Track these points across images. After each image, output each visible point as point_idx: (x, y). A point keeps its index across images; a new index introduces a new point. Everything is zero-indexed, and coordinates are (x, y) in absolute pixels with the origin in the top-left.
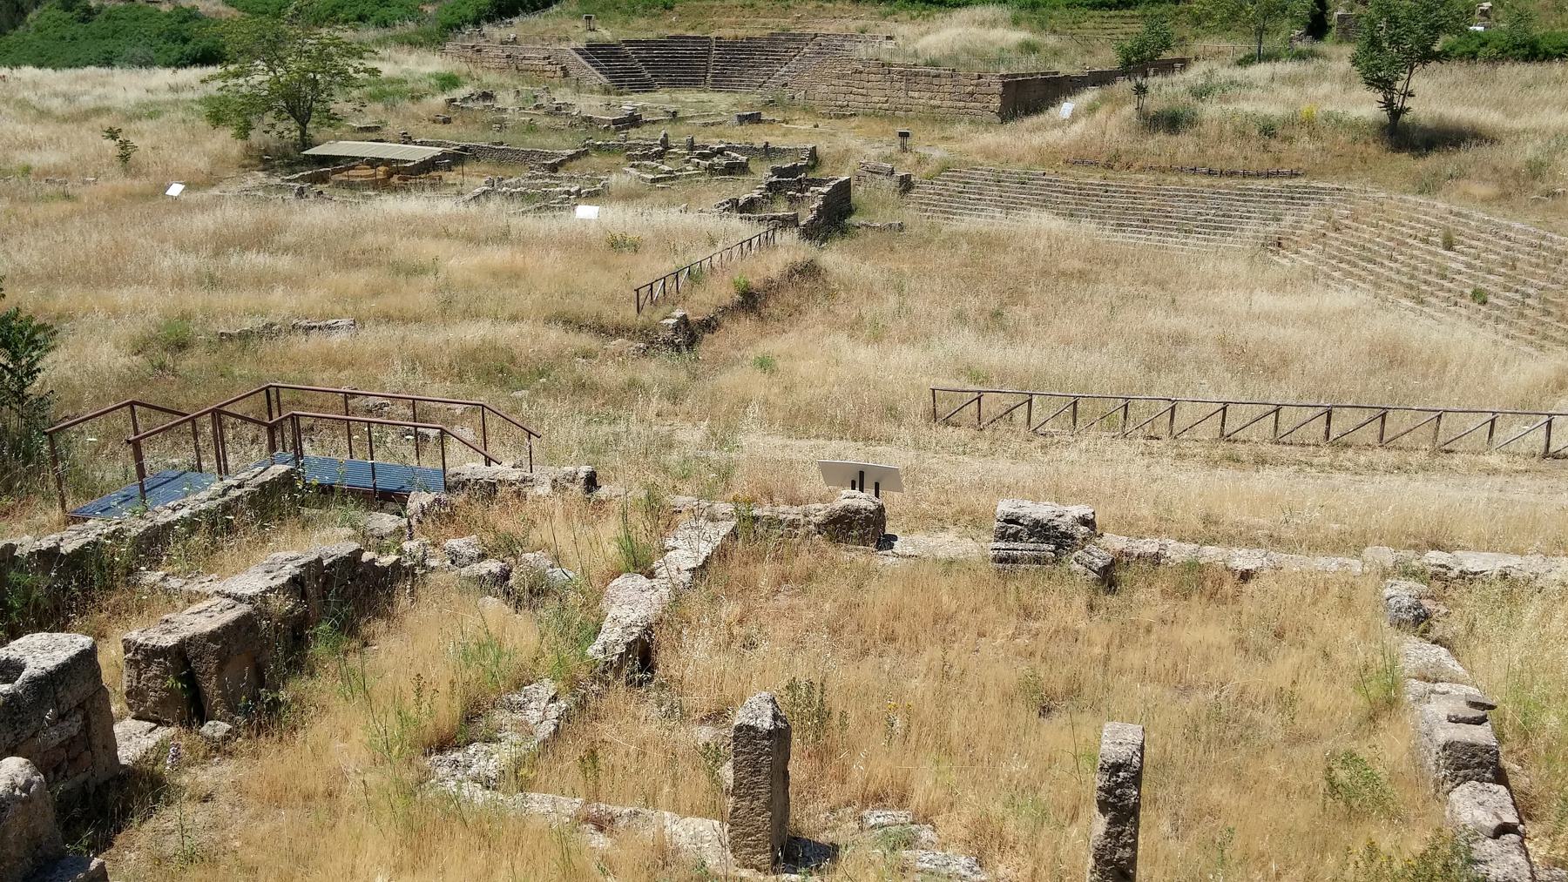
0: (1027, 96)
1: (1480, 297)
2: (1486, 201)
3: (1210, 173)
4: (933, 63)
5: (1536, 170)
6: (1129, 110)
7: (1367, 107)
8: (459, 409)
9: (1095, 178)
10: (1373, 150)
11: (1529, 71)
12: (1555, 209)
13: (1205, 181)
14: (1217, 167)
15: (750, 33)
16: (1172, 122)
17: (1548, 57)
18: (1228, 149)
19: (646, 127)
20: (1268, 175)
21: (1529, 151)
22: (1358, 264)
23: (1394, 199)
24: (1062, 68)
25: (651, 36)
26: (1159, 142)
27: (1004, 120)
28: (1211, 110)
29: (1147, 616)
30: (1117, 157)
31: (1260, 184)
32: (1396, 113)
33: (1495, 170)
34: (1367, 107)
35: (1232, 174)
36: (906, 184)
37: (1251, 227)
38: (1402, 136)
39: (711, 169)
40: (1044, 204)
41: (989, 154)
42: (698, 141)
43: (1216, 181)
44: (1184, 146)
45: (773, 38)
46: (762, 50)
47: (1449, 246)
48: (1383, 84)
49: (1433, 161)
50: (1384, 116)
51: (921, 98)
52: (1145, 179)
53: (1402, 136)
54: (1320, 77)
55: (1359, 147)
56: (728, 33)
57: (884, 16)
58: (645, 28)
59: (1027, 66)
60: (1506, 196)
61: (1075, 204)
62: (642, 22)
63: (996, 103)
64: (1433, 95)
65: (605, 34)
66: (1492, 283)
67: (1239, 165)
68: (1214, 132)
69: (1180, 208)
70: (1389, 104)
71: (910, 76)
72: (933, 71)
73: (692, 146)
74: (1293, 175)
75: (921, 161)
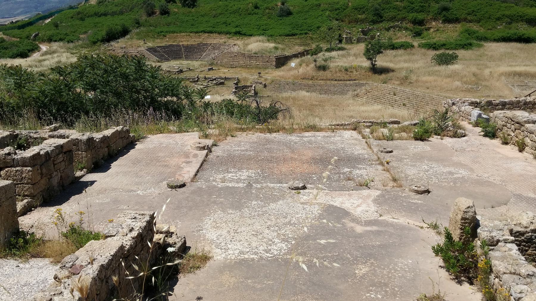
0: (281, 62)
1: (404, 105)
2: (399, 85)
3: (336, 80)
4: (255, 53)
5: (406, 78)
6: (312, 65)
7: (367, 64)
8: (44, 171)
9: (310, 82)
10: (370, 74)
11: (394, 52)
12: (412, 86)
13: (336, 82)
14: (337, 79)
15: (191, 43)
16: (324, 68)
17: (397, 48)
18: (338, 75)
19: (185, 73)
20: (349, 80)
21: (404, 73)
22: (377, 100)
23: (375, 83)
24: (287, 54)
25: (163, 44)
26: (321, 73)
27: (277, 68)
28: (332, 65)
29: (372, 174)
30: (313, 77)
31: (348, 82)
32: (374, 65)
33: (398, 78)
34: (367, 64)
35: (341, 80)
36: (265, 86)
37: (350, 93)
38: (376, 70)
39: (216, 84)
40: (301, 89)
41: (279, 76)
42: (207, 76)
43: (339, 82)
44: (327, 74)
45: (198, 45)
46: (196, 48)
47: (395, 95)
48: (370, 59)
49: (383, 76)
50: (371, 66)
51: (254, 62)
52: (322, 82)
53: (376, 70)
54: (349, 55)
55: (367, 73)
56: (185, 43)
57: (229, 38)
58: (164, 42)
59: (279, 53)
60: (402, 83)
61: (309, 88)
62: (159, 40)
63: (274, 63)
64: (381, 61)
65: (150, 44)
66: (406, 102)
67: (342, 78)
68: (334, 70)
69: (332, 88)
70: (372, 64)
71: (250, 57)
72: (257, 56)
73: (205, 78)
74: (355, 80)
75: (266, 80)
